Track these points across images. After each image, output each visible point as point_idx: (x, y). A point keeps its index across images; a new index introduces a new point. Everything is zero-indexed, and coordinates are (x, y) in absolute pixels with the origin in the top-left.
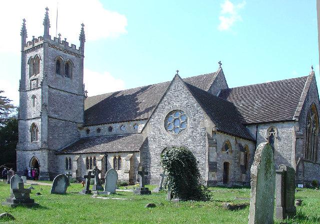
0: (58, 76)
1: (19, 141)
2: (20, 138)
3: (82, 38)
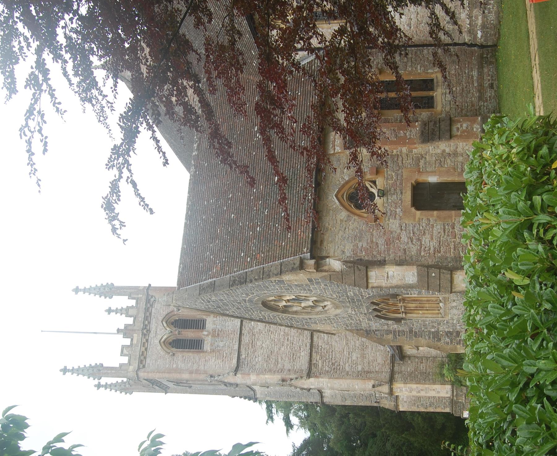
0: (207, 347)
1: (375, 405)
2: (368, 403)
3: (108, 291)
